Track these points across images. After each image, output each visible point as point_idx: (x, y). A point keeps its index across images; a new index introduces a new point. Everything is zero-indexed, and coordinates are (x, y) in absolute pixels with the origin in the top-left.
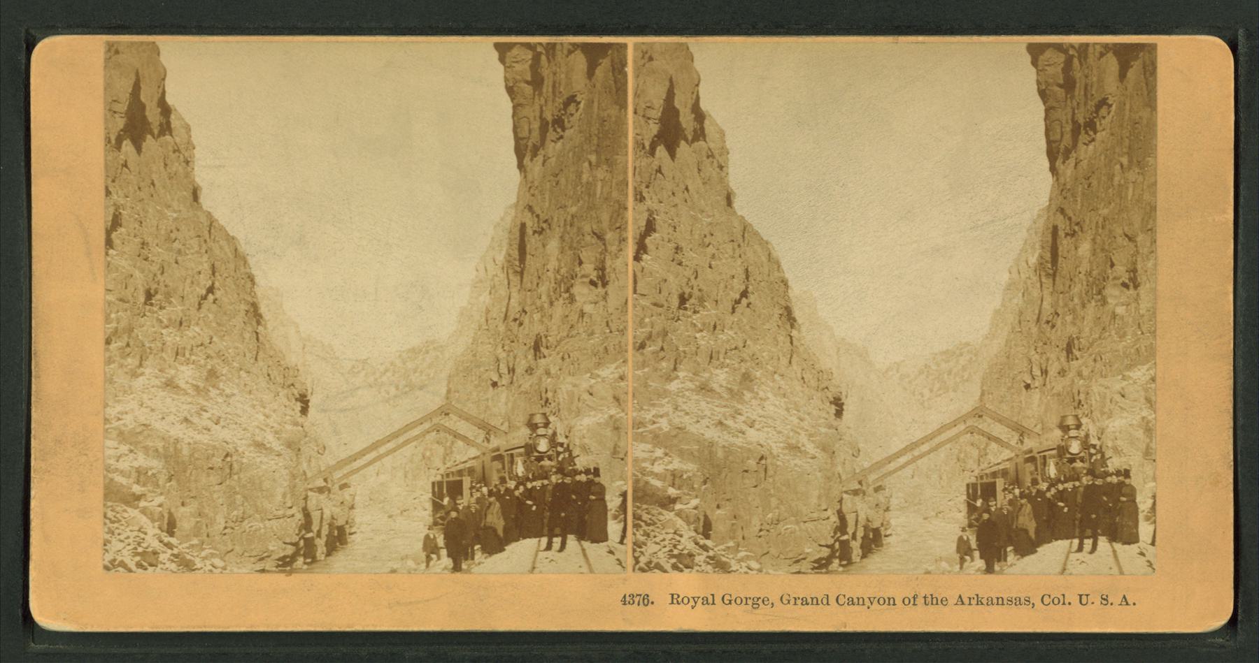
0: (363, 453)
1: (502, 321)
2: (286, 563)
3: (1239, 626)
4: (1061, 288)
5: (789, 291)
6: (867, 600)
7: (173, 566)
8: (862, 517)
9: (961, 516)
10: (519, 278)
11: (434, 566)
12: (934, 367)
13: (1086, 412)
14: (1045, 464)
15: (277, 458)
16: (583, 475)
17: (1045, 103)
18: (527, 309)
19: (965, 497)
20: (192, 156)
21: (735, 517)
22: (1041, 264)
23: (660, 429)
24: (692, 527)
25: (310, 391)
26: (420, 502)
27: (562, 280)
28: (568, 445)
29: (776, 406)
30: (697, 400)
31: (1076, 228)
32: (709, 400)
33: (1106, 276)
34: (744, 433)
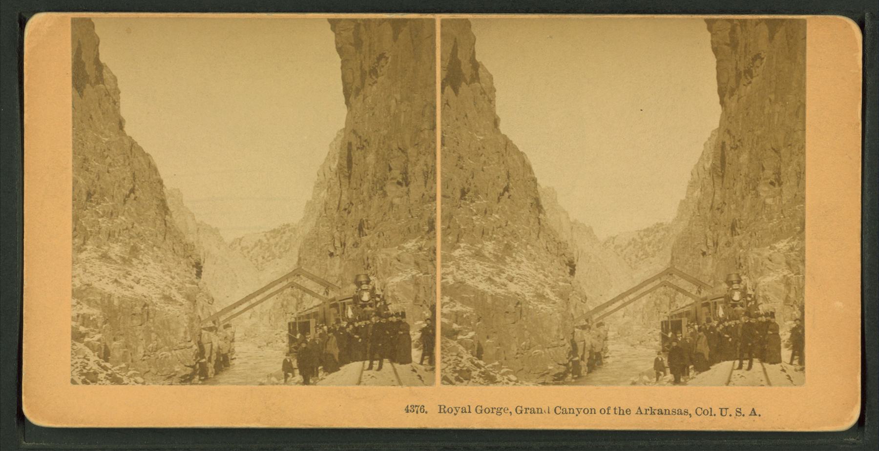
0: (613, 301)
1: (336, 211)
2: (186, 380)
3: (866, 429)
4: (354, 186)
5: (538, 187)
6: (576, 411)
7: (481, 380)
8: (588, 344)
9: (657, 343)
11: (662, 380)
12: (265, 241)
13: (745, 272)
14: (716, 308)
15: (179, 307)
16: (394, 317)
17: (341, 56)
18: (353, 202)
19: (287, 332)
20: (494, 97)
21: (126, 347)
22: (714, 168)
23: (447, 283)
25: (202, 260)
26: (281, 337)
27: (377, 182)
28: (383, 296)
29: (528, 266)
31: (365, 144)
34: (132, 288)
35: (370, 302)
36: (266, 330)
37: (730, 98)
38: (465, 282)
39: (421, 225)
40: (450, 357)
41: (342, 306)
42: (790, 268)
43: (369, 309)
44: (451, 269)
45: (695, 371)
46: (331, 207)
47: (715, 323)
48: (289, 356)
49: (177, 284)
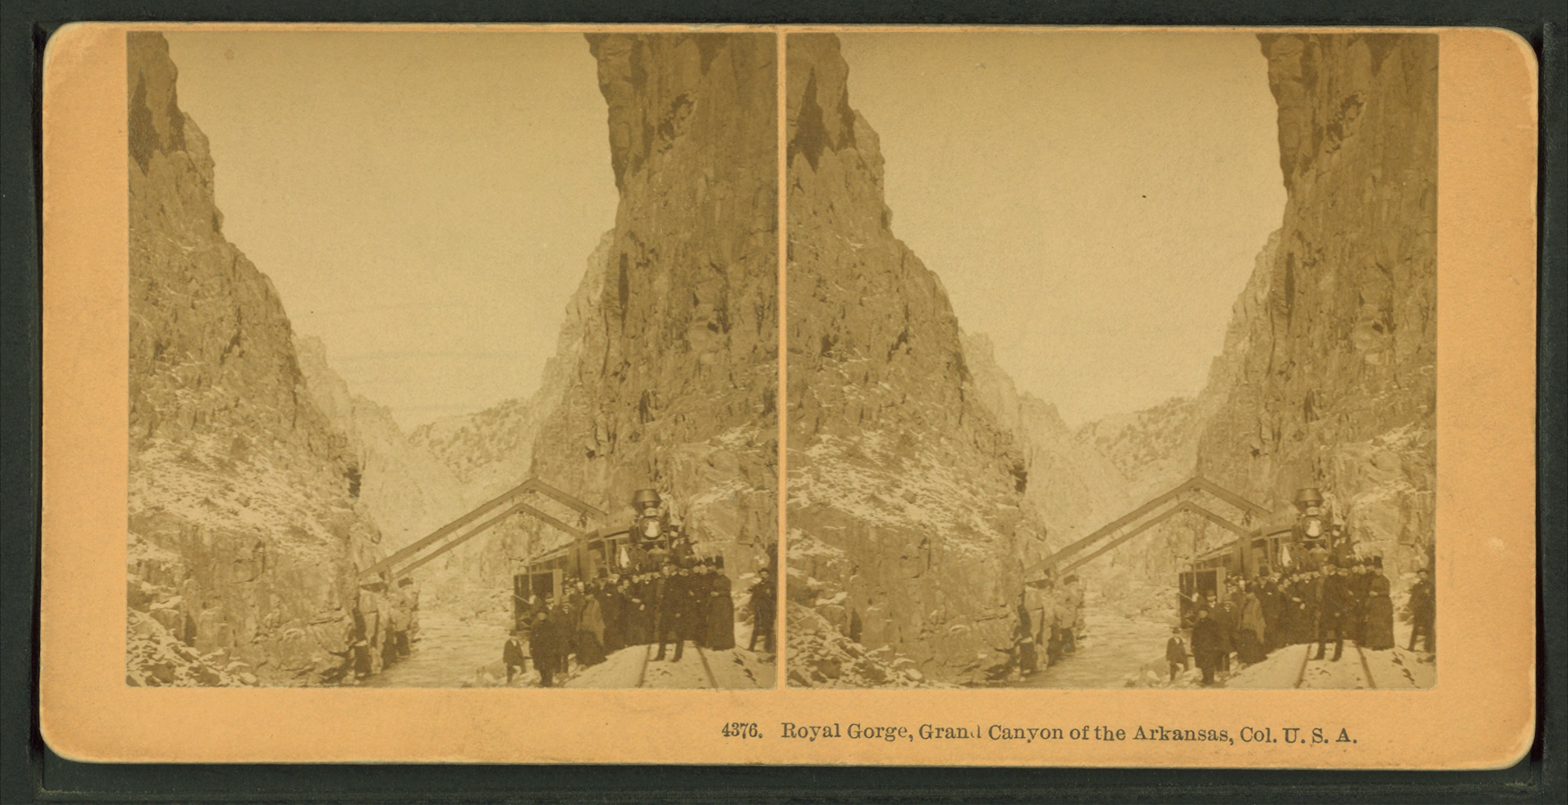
0: (1094, 538)
2: (333, 677)
3: (1545, 767)
4: (632, 331)
5: (959, 333)
7: (858, 678)
8: (1049, 613)
9: (1172, 613)
10: (620, 322)
11: (1181, 678)
12: (474, 431)
13: (1329, 485)
14: (1276, 549)
16: (703, 566)
18: (629, 360)
19: (512, 593)
22: (607, 299)
23: (798, 504)
24: (171, 631)
25: (361, 464)
26: (501, 601)
27: (673, 324)
28: (684, 529)
30: (844, 469)
31: (651, 256)
32: (859, 468)
33: (1354, 317)
35: (1321, 538)
36: (474, 590)
37: (1302, 175)
38: (829, 504)
39: (751, 402)
40: (803, 638)
41: (611, 547)
42: (1410, 478)
43: (658, 551)
44: (804, 480)
45: (1239, 663)
46: (590, 369)
47: (1276, 577)
48: (515, 635)
49: (316, 507)
